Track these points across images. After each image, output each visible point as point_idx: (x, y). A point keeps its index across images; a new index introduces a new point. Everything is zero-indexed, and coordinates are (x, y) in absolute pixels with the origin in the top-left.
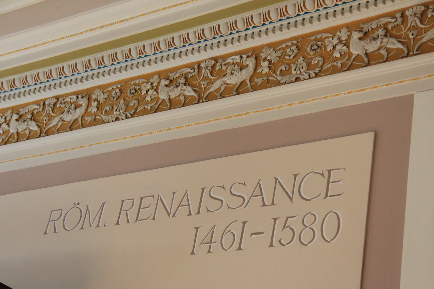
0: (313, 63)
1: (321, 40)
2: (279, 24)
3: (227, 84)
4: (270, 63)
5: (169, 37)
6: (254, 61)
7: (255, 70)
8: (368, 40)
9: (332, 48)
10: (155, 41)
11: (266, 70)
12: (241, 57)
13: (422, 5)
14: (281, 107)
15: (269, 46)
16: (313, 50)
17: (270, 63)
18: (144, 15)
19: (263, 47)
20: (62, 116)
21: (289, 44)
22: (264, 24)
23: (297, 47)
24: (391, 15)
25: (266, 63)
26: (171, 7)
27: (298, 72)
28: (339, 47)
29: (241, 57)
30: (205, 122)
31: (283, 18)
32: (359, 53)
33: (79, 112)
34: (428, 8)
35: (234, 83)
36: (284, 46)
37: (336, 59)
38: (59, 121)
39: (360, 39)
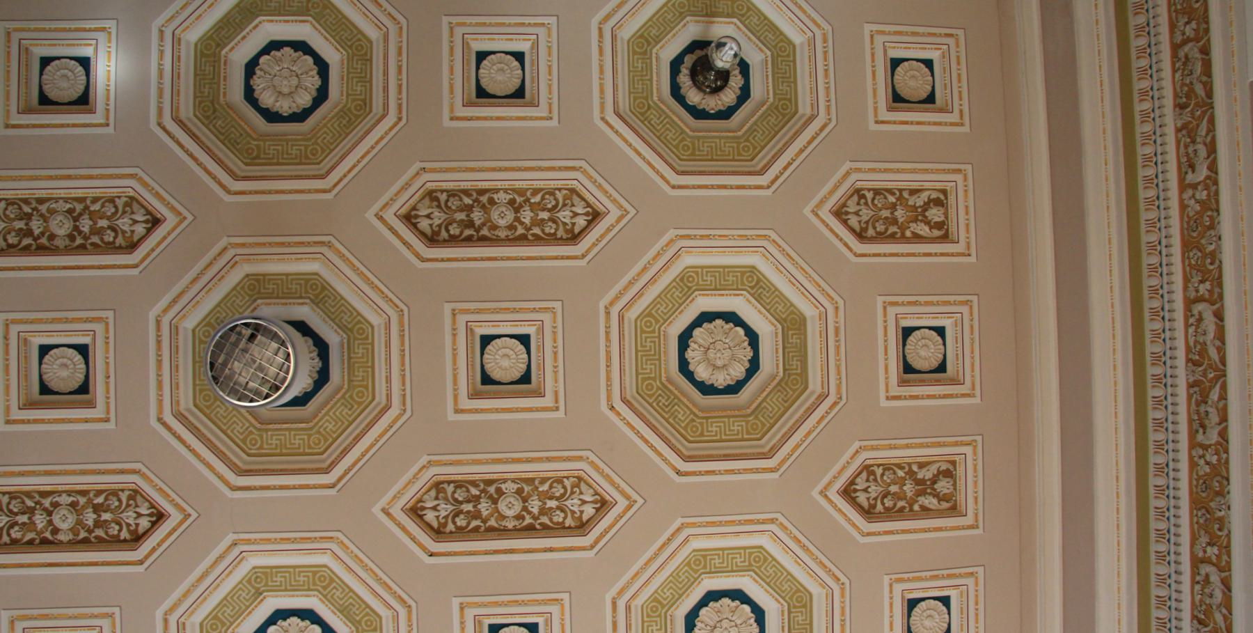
0: (1217, 489)
1: (1199, 478)
2: (1173, 611)
3: (1214, 337)
4: (1209, 544)
5: (1152, 425)
6: (1204, 565)
7: (1214, 564)
8: (1207, 422)
9: (1207, 466)
10: (1155, 623)
11: (1215, 550)
12: (1198, 582)
13: (1192, 621)
14: (1244, 246)
15: (1192, 545)
16: (1197, 228)
17: (1209, 544)
18: (1117, 445)
19: (1192, 553)
20: (1214, 607)
21: (1195, 519)
22: (1168, 519)
23: (1200, 509)
24: (1190, 397)
25: (1209, 549)
26: (1113, 327)
27: (1224, 507)
28: (1208, 457)
29: (1198, 582)
30: (1248, 354)
31: (1160, 270)
32: (1205, 167)
33: (1215, 578)
34: (1196, 617)
35: (1214, 327)
36: (1196, 526)
37: (1219, 460)
38: (1220, 611)
39: (1193, 172)
